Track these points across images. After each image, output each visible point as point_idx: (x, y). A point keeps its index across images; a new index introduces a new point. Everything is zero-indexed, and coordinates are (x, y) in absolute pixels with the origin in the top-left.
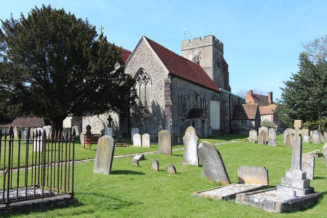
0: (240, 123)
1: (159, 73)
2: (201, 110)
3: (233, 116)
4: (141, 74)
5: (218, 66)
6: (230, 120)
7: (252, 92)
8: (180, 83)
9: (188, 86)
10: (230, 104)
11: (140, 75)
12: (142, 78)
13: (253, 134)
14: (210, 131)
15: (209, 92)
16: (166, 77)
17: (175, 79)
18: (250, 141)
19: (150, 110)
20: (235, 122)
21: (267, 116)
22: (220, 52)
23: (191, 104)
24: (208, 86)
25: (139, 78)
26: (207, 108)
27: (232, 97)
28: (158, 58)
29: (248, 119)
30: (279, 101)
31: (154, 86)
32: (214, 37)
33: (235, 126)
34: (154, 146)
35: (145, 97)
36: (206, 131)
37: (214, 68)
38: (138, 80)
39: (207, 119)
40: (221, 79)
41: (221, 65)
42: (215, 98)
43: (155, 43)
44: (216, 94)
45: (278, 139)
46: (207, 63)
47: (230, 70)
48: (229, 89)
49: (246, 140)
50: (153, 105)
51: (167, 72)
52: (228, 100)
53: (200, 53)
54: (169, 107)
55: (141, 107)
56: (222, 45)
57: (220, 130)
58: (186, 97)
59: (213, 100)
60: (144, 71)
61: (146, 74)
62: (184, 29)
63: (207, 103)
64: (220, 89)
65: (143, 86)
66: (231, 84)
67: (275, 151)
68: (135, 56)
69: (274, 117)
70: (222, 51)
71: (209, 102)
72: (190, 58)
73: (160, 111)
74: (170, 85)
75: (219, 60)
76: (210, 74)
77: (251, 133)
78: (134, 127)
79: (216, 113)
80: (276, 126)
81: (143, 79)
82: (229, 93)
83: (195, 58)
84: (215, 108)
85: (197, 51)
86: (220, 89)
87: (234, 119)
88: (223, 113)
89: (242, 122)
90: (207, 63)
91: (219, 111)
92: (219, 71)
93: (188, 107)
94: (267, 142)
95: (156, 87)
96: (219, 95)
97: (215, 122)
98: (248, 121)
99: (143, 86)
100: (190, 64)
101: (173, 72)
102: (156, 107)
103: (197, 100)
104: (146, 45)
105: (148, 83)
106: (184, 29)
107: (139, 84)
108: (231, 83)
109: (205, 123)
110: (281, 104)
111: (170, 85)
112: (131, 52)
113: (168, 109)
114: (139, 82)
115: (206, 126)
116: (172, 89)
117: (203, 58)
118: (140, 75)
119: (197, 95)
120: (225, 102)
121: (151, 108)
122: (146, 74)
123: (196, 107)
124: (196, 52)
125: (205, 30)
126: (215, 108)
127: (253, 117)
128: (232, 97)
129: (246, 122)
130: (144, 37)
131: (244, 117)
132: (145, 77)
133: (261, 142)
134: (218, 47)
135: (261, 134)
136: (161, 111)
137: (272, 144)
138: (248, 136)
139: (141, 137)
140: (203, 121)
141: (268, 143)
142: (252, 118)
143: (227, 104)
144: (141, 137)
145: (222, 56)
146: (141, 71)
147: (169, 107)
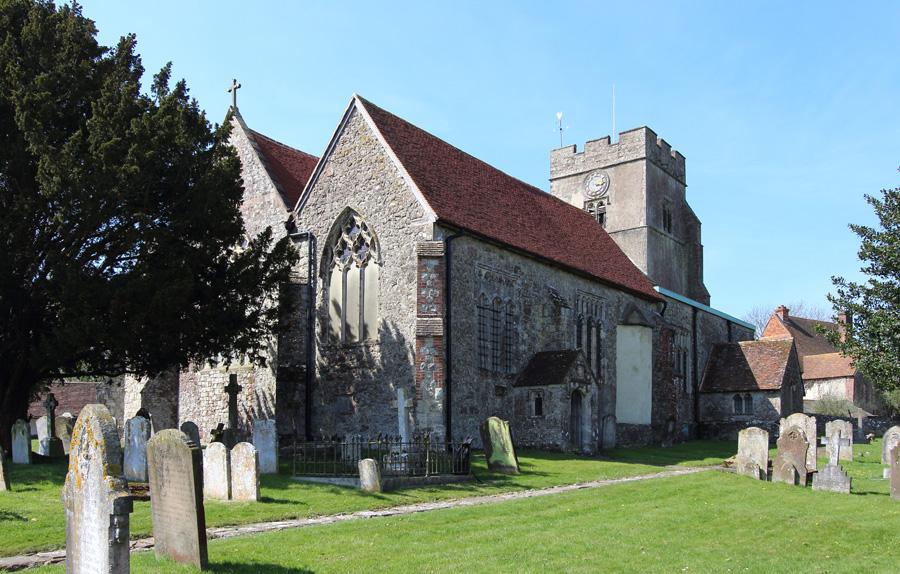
0: (730, 402)
1: (408, 219)
2: (570, 357)
3: (709, 380)
4: (348, 231)
5: (668, 225)
6: (696, 393)
7: (786, 311)
8: (489, 260)
9: (525, 270)
10: (694, 337)
11: (345, 236)
12: (350, 244)
13: (752, 444)
14: (610, 429)
15: (612, 295)
16: (428, 235)
17: (463, 246)
18: (741, 469)
19: (376, 353)
20: (710, 392)
21: (834, 383)
22: (672, 182)
23: (534, 335)
24: (607, 276)
25: (344, 244)
26: (604, 353)
27: (703, 320)
28: (402, 172)
29: (758, 390)
30: (846, 290)
31: (389, 271)
32: (651, 135)
33: (712, 412)
34: (275, 494)
35: (361, 314)
36: (587, 429)
37: (652, 230)
38: (340, 253)
39: (593, 388)
40: (675, 266)
41: (675, 222)
42: (635, 318)
43: (407, 125)
44: (641, 304)
45: (860, 461)
46: (628, 219)
47: (706, 238)
48: (704, 297)
49: (727, 465)
50: (383, 337)
51: (431, 216)
52: (689, 327)
53: (607, 185)
54: (430, 342)
55: (349, 346)
56: (680, 160)
57: (655, 426)
58: (516, 311)
59: (626, 323)
60: (358, 221)
61: (365, 228)
62: (559, 116)
63: (603, 335)
64: (657, 288)
65: (354, 271)
66: (709, 280)
67: (836, 528)
68: (330, 169)
69: (857, 386)
70: (680, 177)
71: (613, 332)
72: (577, 201)
73: (406, 357)
74: (435, 263)
75: (670, 208)
76: (637, 254)
77: (743, 437)
78: (743, 425)
79: (635, 369)
80: (860, 415)
81: (357, 249)
82: (704, 307)
83: (590, 203)
84: (633, 353)
85: (599, 181)
86: (657, 288)
87: (709, 390)
88: (664, 368)
89: (738, 399)
90: (628, 219)
91: (649, 362)
92: (669, 242)
93: (523, 348)
94: (810, 476)
95: (397, 274)
96: (652, 307)
97: (635, 402)
98: (757, 398)
99: (354, 271)
100: (547, 206)
101: (457, 217)
102: (393, 344)
103: (557, 322)
104: (365, 129)
105: (371, 262)
106: (559, 116)
107: (342, 266)
108: (712, 277)
109: (586, 401)
110: (859, 301)
111: (435, 263)
112: (313, 160)
113: (426, 350)
114: (343, 261)
115: (587, 412)
116: (444, 273)
117: (617, 201)
118: (345, 236)
119: (558, 304)
120: (673, 333)
121: (377, 348)
122: (365, 228)
123: (554, 347)
124: (595, 184)
125: (627, 112)
126: (633, 353)
127: (776, 383)
128: (703, 320)
129: (749, 399)
130: (358, 103)
131: (744, 383)
132: (361, 240)
133: (786, 474)
134: (665, 168)
135: (787, 446)
136: (410, 356)
137: (831, 482)
138: (732, 449)
139: (229, 458)
140: (576, 398)
141: (815, 478)
142: (770, 386)
143: (684, 341)
144: (229, 458)
145: (680, 195)
146: (347, 220)
147: (430, 342)
